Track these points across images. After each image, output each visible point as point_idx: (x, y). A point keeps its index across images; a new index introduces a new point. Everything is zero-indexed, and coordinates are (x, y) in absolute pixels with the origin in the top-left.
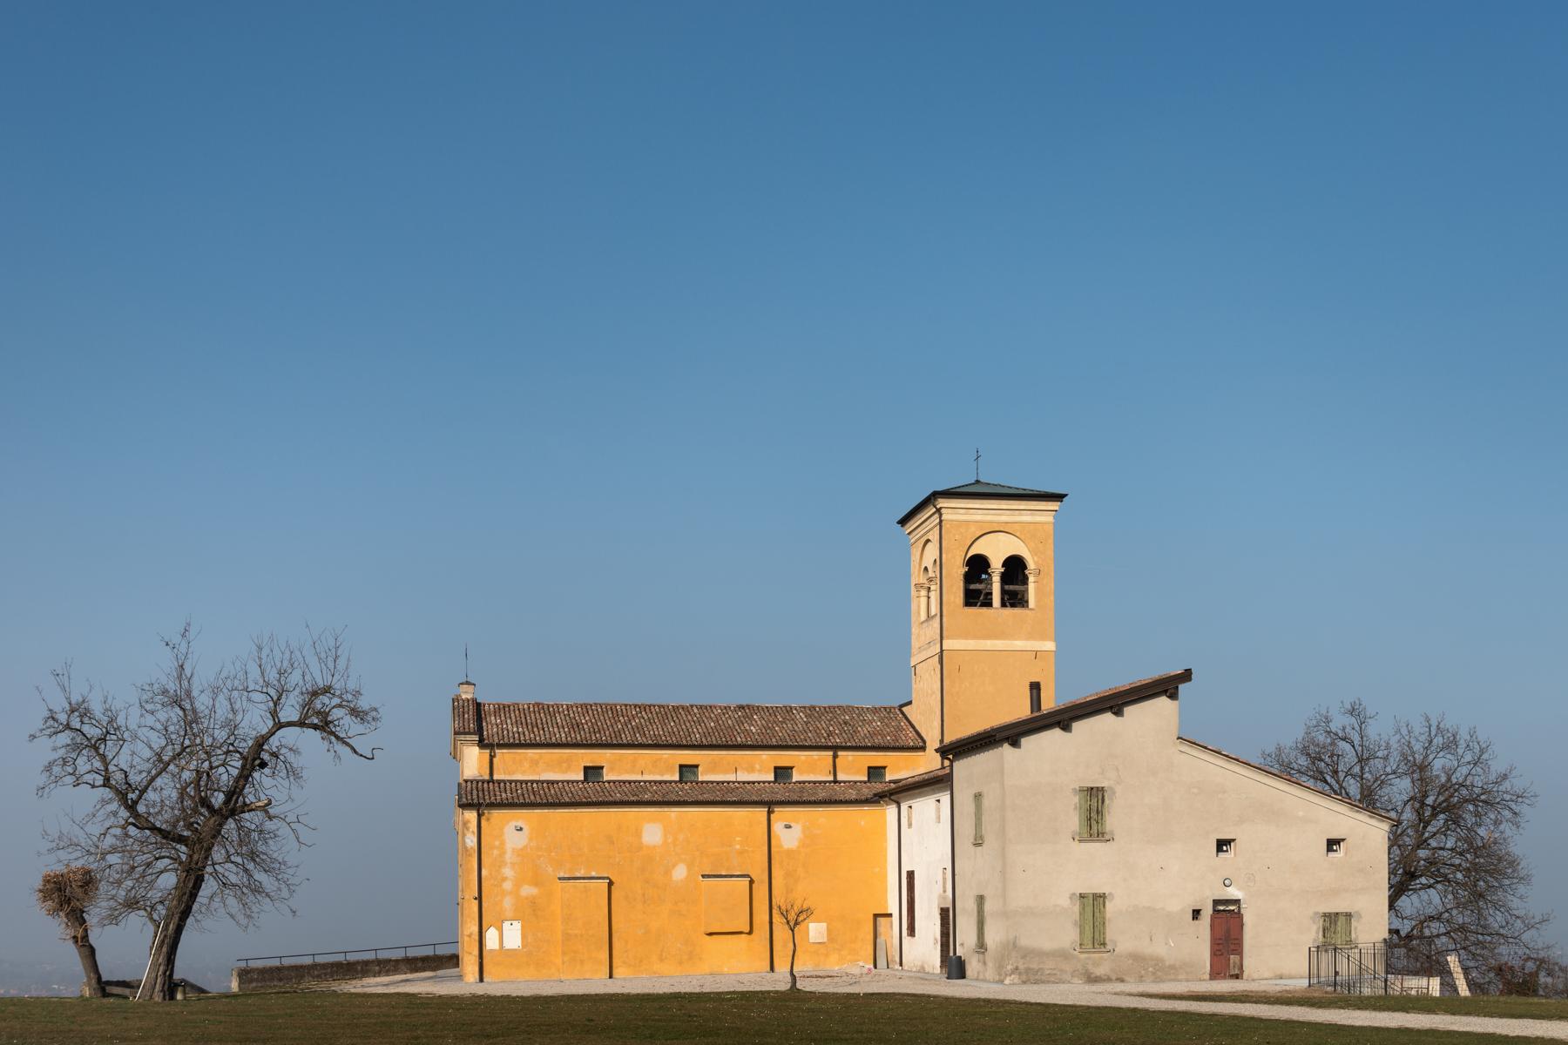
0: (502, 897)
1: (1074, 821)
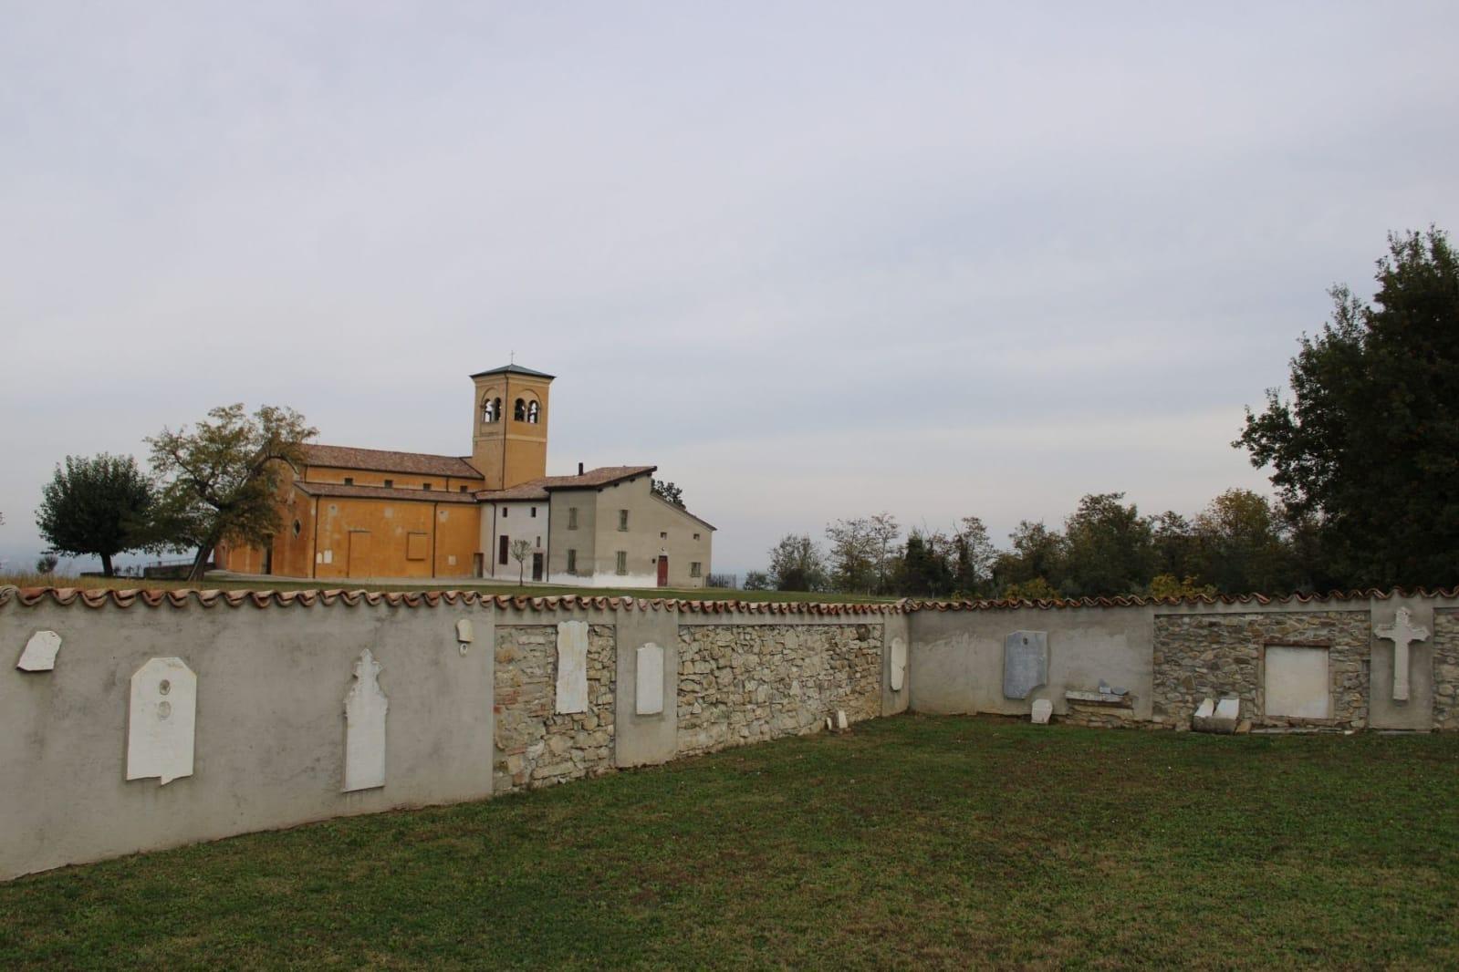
0: (325, 540)
1: (618, 522)
